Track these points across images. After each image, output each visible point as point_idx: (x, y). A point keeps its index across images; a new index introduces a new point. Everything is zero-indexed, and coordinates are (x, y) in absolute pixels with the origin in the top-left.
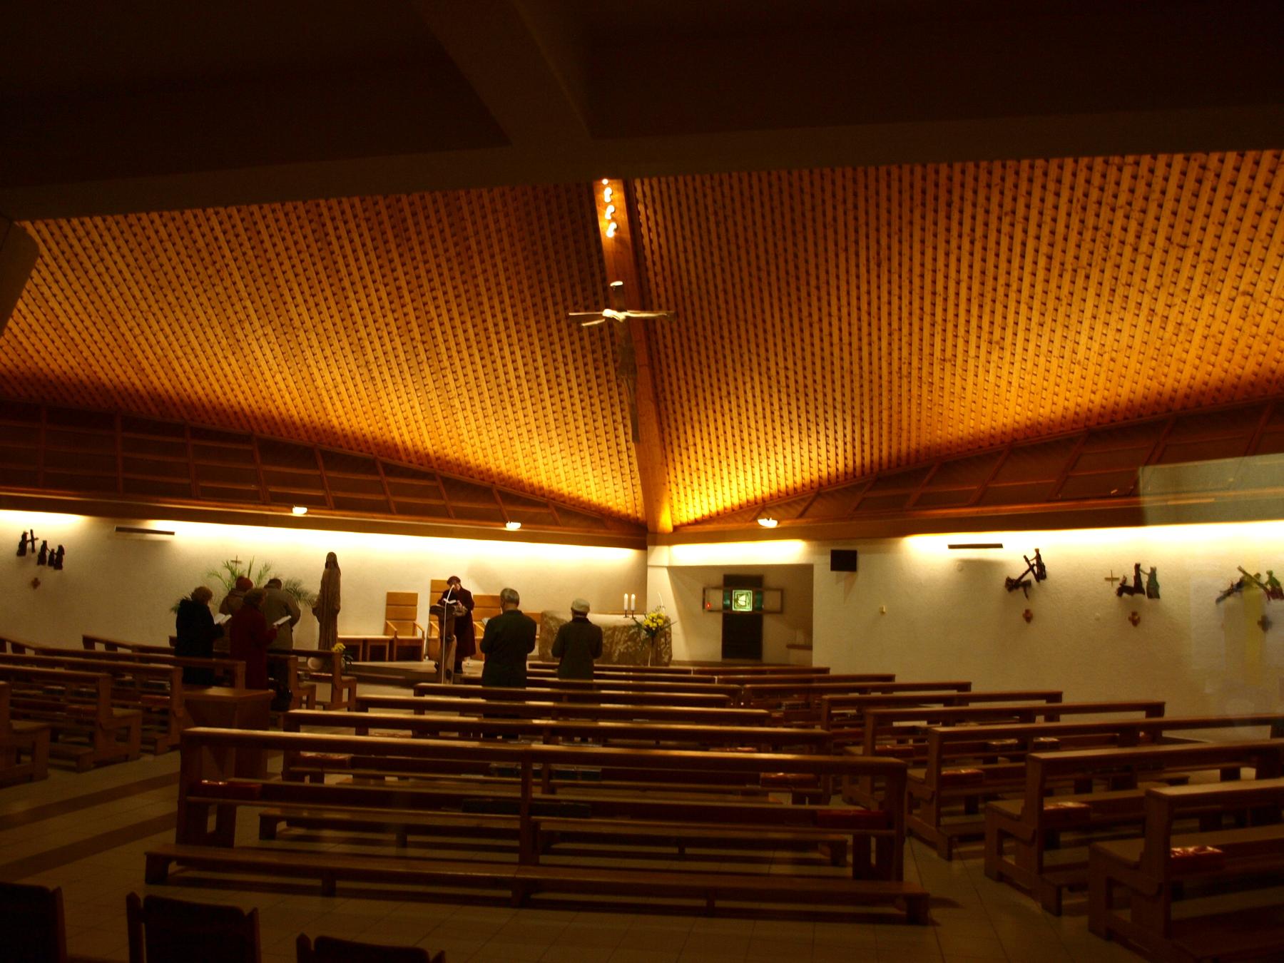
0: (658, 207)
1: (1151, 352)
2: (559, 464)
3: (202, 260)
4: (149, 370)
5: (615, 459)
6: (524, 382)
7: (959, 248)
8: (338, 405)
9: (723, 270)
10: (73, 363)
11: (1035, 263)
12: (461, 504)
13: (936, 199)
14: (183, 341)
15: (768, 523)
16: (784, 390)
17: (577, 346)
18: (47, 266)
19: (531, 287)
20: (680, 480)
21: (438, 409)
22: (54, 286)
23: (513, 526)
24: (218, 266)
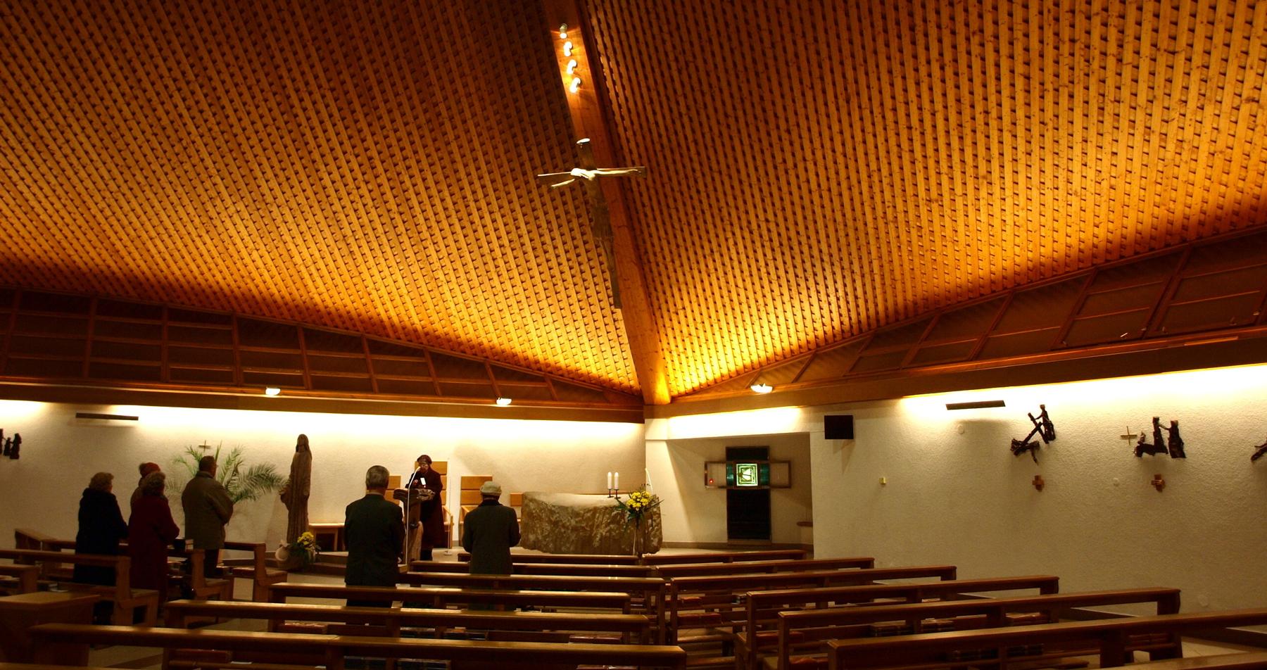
0: (620, 58)
1: (1153, 175)
2: (554, 335)
3: (168, 137)
4: (123, 252)
5: (611, 328)
6: (508, 251)
7: (930, 75)
8: (319, 282)
9: (691, 120)
10: (46, 246)
11: (1013, 85)
12: (449, 381)
13: (898, 23)
14: (155, 221)
15: (762, 389)
16: (767, 244)
17: (561, 211)
18: (13, 149)
19: (507, 152)
20: (673, 347)
21: (421, 282)
22: (21, 169)
23: (504, 403)
24: (184, 143)
